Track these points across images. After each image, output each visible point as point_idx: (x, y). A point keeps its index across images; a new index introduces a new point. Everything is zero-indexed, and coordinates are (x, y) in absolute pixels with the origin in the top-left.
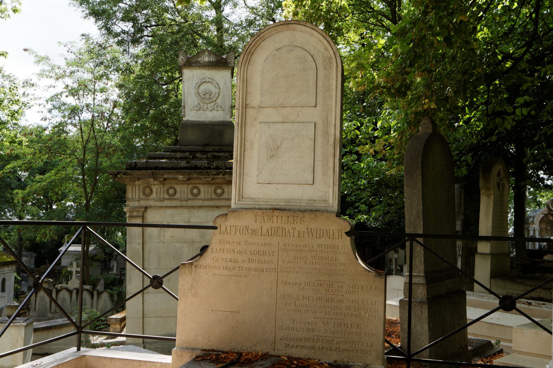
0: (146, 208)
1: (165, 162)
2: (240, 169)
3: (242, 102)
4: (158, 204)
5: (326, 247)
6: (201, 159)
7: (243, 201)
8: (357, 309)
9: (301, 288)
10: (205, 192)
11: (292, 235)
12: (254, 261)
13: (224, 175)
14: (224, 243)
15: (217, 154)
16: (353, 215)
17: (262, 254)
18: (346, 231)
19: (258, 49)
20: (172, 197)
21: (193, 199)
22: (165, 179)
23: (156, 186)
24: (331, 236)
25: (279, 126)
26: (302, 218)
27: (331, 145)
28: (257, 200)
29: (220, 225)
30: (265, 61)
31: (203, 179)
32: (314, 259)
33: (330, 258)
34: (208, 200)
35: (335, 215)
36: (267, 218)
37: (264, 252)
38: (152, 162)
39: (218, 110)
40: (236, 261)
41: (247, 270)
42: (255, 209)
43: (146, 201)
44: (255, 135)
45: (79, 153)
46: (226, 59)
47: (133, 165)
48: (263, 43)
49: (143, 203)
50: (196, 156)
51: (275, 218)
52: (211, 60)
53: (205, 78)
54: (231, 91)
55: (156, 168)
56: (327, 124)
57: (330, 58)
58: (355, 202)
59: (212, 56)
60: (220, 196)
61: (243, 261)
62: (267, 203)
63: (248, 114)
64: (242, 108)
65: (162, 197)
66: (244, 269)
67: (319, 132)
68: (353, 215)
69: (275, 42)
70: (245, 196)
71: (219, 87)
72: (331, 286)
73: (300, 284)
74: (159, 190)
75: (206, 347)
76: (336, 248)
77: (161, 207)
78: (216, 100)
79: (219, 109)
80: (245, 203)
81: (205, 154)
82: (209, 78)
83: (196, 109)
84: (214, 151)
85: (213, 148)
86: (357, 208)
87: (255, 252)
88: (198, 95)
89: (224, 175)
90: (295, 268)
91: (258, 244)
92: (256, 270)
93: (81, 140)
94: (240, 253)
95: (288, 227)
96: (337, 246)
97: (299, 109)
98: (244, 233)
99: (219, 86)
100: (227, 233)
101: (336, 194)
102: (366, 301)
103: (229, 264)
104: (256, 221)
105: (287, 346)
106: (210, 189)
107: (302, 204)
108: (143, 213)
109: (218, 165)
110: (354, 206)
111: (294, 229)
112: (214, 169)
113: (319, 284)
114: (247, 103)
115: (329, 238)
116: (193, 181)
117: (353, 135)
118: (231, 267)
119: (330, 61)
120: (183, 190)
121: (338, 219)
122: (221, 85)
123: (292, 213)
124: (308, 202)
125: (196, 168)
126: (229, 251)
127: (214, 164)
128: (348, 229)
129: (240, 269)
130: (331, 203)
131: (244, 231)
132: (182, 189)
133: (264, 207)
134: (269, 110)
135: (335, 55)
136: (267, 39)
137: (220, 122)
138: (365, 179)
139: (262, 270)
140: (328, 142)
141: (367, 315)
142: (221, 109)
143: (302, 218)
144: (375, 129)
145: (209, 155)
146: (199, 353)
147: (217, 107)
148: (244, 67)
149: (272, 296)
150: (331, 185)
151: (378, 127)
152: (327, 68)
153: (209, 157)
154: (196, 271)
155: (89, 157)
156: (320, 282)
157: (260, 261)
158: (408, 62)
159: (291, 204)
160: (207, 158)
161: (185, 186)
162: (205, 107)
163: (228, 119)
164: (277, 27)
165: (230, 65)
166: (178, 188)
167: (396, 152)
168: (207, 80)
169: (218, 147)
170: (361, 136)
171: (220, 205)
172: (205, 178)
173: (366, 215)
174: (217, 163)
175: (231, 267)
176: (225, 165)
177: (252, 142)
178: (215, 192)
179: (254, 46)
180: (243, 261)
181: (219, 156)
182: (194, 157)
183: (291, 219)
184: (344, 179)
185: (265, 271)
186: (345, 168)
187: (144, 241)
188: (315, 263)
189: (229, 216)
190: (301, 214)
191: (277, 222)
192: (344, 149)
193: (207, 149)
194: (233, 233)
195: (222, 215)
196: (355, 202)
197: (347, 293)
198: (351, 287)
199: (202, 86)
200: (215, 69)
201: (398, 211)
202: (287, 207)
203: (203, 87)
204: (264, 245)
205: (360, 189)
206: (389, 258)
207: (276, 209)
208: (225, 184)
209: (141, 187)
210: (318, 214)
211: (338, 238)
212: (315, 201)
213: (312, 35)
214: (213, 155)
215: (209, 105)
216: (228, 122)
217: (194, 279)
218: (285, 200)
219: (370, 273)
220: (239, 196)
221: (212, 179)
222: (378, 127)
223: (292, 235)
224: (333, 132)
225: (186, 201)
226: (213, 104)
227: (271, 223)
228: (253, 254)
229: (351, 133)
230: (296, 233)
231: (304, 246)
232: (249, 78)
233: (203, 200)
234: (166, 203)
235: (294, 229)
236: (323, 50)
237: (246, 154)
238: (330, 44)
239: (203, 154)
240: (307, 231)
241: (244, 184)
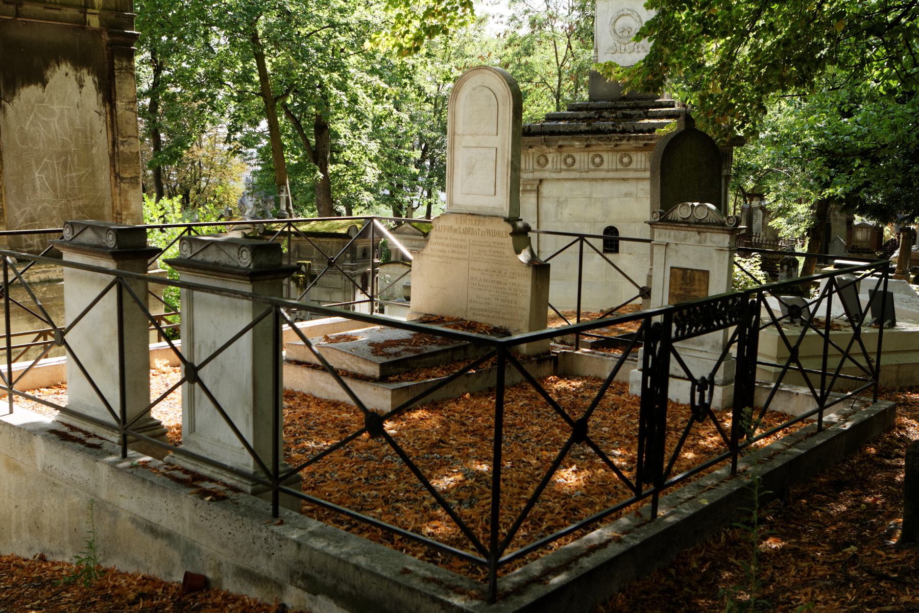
0: (541, 181)
1: (563, 126)
4: (554, 175)
6: (608, 119)
13: (628, 140)
20: (570, 167)
21: (594, 170)
22: (560, 147)
23: (552, 155)
25: (474, 150)
34: (612, 170)
38: (548, 126)
43: (541, 173)
45: (554, 82)
47: (526, 130)
49: (538, 175)
50: (603, 115)
55: (552, 133)
60: (626, 166)
61: (449, 252)
65: (559, 167)
67: (499, 155)
70: (454, 203)
74: (555, 160)
75: (428, 312)
77: (558, 179)
79: (640, 50)
83: (612, 51)
88: (613, 34)
89: (628, 140)
92: (456, 258)
93: (554, 60)
94: (447, 245)
95: (475, 228)
103: (440, 254)
105: (474, 314)
108: (538, 187)
116: (594, 148)
120: (582, 158)
125: (598, 131)
127: (621, 126)
132: (582, 157)
145: (619, 113)
146: (421, 316)
155: (568, 84)
161: (586, 154)
162: (623, 48)
166: (577, 156)
168: (626, 12)
172: (606, 145)
178: (621, 162)
180: (449, 252)
182: (600, 117)
183: (477, 223)
187: (540, 219)
191: (469, 224)
199: (619, 21)
202: (478, 213)
203: (620, 23)
209: (536, 156)
215: (627, 46)
225: (586, 172)
234: (564, 175)
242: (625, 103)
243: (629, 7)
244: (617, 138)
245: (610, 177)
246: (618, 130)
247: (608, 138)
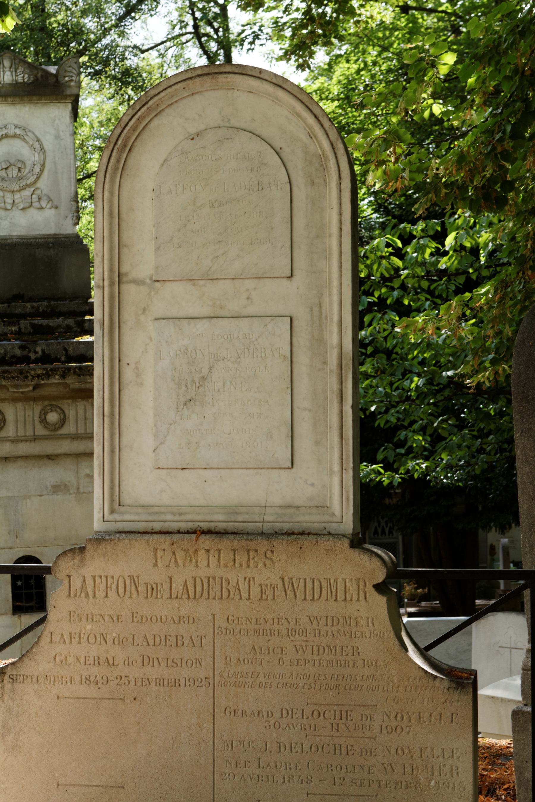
2: (112, 434)
3: (111, 270)
5: (330, 623)
7: (123, 513)
8: (408, 769)
9: (272, 722)
10: (17, 422)
11: (245, 595)
12: (155, 660)
13: (63, 376)
14: (80, 620)
15: (44, 322)
16: (394, 461)
17: (174, 643)
18: (376, 582)
19: (144, 136)
24: (341, 596)
25: (202, 326)
26: (269, 554)
27: (331, 371)
28: (156, 509)
29: (69, 576)
30: (163, 165)
31: (11, 390)
32: (301, 652)
33: (338, 649)
35: (347, 542)
36: (183, 554)
37: (179, 638)
39: (42, 208)
40: (111, 662)
41: (139, 684)
42: (153, 533)
44: (146, 351)
46: (56, 76)
48: (156, 122)
51: (202, 554)
52: (20, 79)
53: (5, 127)
54: (72, 157)
56: (320, 319)
57: (322, 158)
58: (397, 428)
59: (20, 69)
60: (55, 430)
61: (128, 663)
62: (182, 518)
63: (125, 297)
64: (112, 284)
66: (133, 682)
68: (394, 461)
69: (187, 119)
70: (127, 499)
71: (42, 148)
72: (344, 716)
73: (270, 714)
76: (353, 624)
78: (35, 182)
79: (44, 204)
80: (127, 517)
81: (13, 324)
82: (16, 127)
84: (36, 314)
85: (33, 307)
86: (402, 444)
87: (158, 639)
89: (63, 376)
90: (255, 675)
91: (164, 618)
92: (160, 682)
94: (121, 642)
96: (356, 618)
97: (250, 284)
98: (128, 593)
99: (41, 145)
100: (87, 596)
101: (347, 492)
102: (429, 750)
103: (95, 671)
104: (156, 565)
106: (29, 413)
107: (267, 518)
109: (47, 352)
110: (396, 439)
111: (249, 580)
112: (36, 361)
113: (316, 713)
114: (123, 271)
115: (336, 600)
117: (387, 269)
118: (99, 678)
119: (322, 165)
121: (356, 555)
122: (48, 143)
123: (243, 543)
124: (280, 511)
126: (92, 639)
127: (39, 349)
128: (380, 576)
129: (122, 681)
130: (337, 512)
131: (128, 588)
133: (174, 526)
134: (179, 288)
135: (334, 149)
136: (167, 111)
137: (48, 237)
138: (419, 375)
139: (177, 684)
140: (325, 363)
141: (433, 783)
142: (49, 205)
143: (269, 554)
144: (440, 253)
145: (24, 324)
147: (40, 199)
148: (112, 181)
149: (203, 744)
150: (336, 468)
151: (447, 248)
152: (317, 180)
153: (23, 330)
154: (13, 690)
156: (316, 707)
157: (170, 661)
158: (509, 128)
159: (240, 518)
160: (19, 334)
162: (9, 200)
163: (67, 229)
164: (190, 82)
165: (68, 92)
167: (490, 332)
168: (11, 130)
169: (45, 303)
170: (406, 272)
171: (56, 452)
172: (16, 386)
173: (426, 459)
174: (44, 347)
175: (99, 678)
176: (66, 350)
177: (137, 368)
178: (44, 421)
179: (134, 129)
180: (128, 663)
181: (48, 327)
183: (241, 557)
184: (367, 376)
185: (182, 685)
186: (370, 350)
188: (303, 662)
189: (89, 553)
190: (265, 542)
192: (364, 297)
193: (19, 308)
194: (101, 594)
195: (71, 550)
196: (397, 428)
197: (384, 731)
198: (392, 717)
200: (30, 101)
201: (506, 446)
202: (231, 526)
204: (177, 621)
205: (408, 398)
206: (489, 543)
207: (204, 532)
208: (68, 398)
210: (307, 541)
211: (358, 600)
212: (298, 507)
213: (277, 100)
214: (33, 326)
215: (17, 196)
216: (67, 237)
217: (9, 710)
218: (224, 507)
219: (437, 683)
220: (112, 500)
221: (35, 388)
222: (447, 248)
223: (245, 595)
224: (335, 339)
226: (27, 193)
227: (192, 567)
228: (151, 643)
229: (380, 264)
230: (255, 590)
231: (276, 621)
232: (124, 208)
233: (13, 441)
235: (249, 580)
236: (304, 137)
237: (125, 397)
238: (320, 122)
239: (10, 324)
240: (280, 586)
241: (123, 470)
242: (28, 305)
243: (16, 122)
244: (39, 372)
245: (21, 453)
246: (33, 357)
247: (21, 372)
